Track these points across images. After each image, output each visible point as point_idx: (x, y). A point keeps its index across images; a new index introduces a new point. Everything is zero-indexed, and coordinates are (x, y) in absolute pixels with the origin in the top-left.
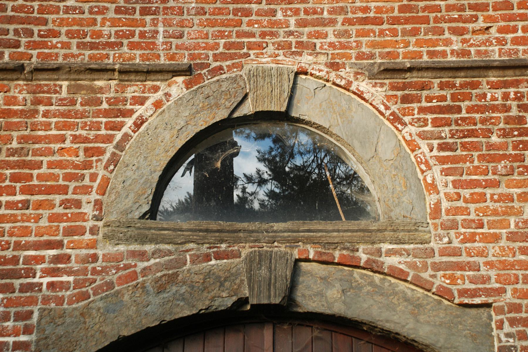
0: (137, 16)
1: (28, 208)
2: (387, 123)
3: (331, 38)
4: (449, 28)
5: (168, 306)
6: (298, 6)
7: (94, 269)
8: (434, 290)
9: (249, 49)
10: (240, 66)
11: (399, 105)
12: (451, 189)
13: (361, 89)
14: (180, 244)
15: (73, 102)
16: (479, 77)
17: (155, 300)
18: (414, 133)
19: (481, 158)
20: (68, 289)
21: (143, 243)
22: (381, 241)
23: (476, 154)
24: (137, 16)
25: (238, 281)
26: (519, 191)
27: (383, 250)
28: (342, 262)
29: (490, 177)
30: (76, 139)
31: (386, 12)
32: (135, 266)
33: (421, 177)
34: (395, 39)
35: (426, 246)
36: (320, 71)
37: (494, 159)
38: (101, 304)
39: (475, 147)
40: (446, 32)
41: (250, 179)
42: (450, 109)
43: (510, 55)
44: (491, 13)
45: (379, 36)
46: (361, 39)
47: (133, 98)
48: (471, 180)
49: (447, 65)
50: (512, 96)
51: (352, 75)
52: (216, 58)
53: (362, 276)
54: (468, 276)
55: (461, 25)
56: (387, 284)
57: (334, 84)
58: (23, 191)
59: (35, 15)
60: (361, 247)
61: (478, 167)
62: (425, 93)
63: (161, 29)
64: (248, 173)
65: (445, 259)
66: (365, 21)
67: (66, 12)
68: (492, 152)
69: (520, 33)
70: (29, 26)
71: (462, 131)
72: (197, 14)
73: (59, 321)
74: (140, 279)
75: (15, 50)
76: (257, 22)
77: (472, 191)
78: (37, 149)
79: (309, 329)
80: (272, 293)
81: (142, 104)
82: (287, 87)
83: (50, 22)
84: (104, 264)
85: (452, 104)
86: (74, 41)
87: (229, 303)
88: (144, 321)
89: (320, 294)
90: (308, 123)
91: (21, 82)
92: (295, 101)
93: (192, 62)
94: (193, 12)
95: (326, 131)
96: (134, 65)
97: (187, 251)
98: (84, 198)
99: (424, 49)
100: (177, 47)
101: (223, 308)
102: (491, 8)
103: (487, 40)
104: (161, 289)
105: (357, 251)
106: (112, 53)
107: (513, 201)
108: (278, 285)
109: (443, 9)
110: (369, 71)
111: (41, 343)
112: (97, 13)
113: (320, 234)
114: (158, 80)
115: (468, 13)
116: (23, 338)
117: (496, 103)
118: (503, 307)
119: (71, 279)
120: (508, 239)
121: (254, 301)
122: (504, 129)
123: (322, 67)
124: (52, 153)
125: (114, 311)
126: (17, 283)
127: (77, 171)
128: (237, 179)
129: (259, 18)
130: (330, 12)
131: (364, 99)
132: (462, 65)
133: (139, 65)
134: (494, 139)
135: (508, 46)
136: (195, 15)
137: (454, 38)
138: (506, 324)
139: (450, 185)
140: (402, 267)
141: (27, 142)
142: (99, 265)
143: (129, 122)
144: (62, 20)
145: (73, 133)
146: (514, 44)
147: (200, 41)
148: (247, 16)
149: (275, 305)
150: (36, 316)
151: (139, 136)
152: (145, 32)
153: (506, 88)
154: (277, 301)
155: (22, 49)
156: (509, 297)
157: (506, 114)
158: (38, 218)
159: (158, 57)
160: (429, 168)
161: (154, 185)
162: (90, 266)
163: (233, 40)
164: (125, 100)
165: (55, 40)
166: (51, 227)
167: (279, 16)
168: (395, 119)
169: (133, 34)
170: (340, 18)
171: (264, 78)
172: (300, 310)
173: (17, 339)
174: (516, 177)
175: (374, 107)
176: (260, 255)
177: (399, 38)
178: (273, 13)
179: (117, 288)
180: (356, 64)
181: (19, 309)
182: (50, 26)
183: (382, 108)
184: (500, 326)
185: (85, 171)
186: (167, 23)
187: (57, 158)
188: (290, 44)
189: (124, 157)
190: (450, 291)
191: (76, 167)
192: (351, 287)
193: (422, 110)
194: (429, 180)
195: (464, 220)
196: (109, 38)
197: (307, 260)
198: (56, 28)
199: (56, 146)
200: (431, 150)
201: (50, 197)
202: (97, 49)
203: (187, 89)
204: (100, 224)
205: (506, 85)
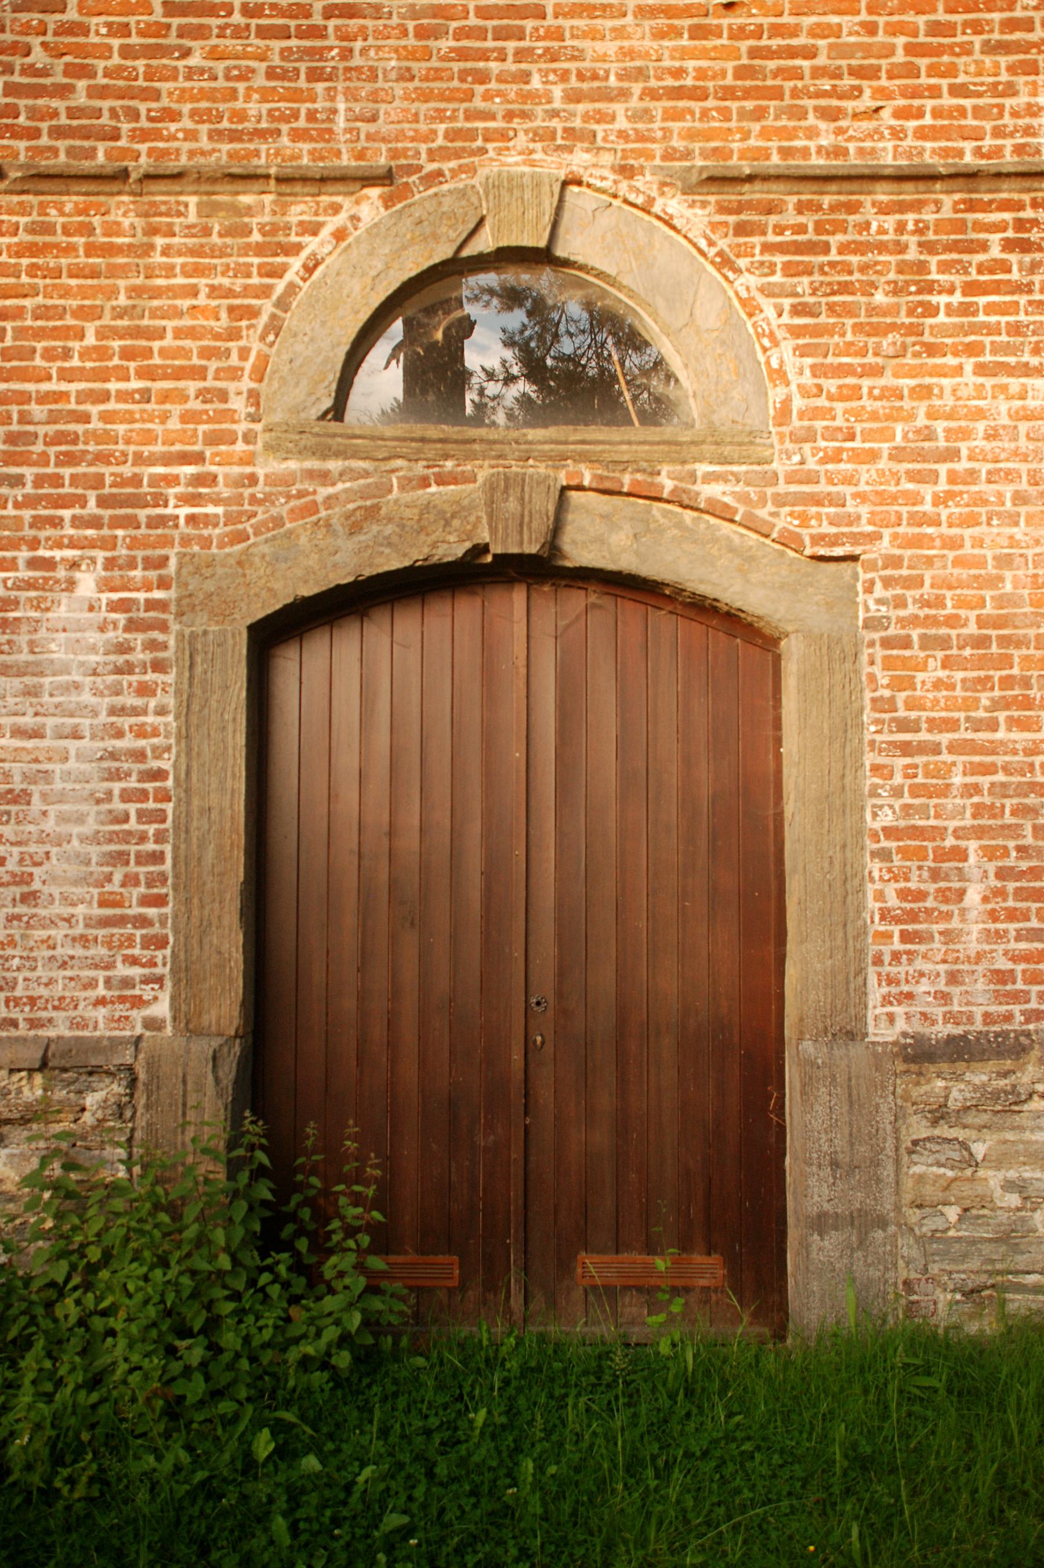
0: (302, 83)
1: (148, 401)
2: (710, 268)
3: (622, 123)
4: (816, 109)
5: (367, 554)
6: (566, 65)
7: (253, 496)
8: (774, 535)
9: (486, 140)
10: (472, 170)
11: (731, 239)
12: (807, 379)
13: (669, 210)
14: (384, 459)
15: (207, 232)
16: (861, 193)
18: (753, 286)
19: (858, 328)
20: (216, 525)
21: (324, 457)
22: (695, 460)
23: (849, 322)
24: (302, 83)
25: (472, 519)
26: (912, 382)
27: (699, 474)
28: (635, 491)
29: (870, 359)
30: (214, 291)
31: (714, 78)
32: (315, 492)
33: (762, 359)
34: (726, 125)
35: (766, 467)
36: (603, 179)
38: (266, 549)
39: (849, 310)
40: (811, 115)
41: (490, 376)
42: (811, 248)
43: (910, 156)
44: (884, 82)
45: (701, 119)
46: (670, 124)
47: (301, 223)
48: (841, 365)
49: (810, 172)
50: (910, 226)
51: (655, 187)
52: (432, 154)
53: (665, 513)
54: (828, 515)
55: (835, 102)
56: (703, 526)
57: (626, 201)
58: (141, 374)
59: (141, 82)
60: (665, 469)
61: (851, 344)
62: (773, 219)
63: (341, 106)
64: (488, 366)
65: (793, 488)
66: (677, 93)
67: (188, 78)
68: (874, 320)
69: (928, 120)
70: (131, 103)
71: (830, 284)
72: (401, 78)
73: (207, 572)
74: (323, 513)
75: (112, 144)
76: (499, 93)
77: (841, 382)
78: (157, 308)
79: (582, 593)
80: (526, 537)
81: (315, 234)
82: (548, 206)
83: (164, 94)
84: (268, 489)
85: (815, 238)
86: (204, 128)
87: (459, 551)
88: (331, 576)
89: (601, 540)
90: (582, 268)
91: (126, 198)
92: (562, 230)
93: (393, 163)
94: (393, 75)
95: (612, 281)
96: (300, 167)
97: (393, 471)
98: (231, 386)
99: (774, 144)
100: (369, 137)
101: (450, 559)
102: (883, 74)
103: (876, 131)
104: (355, 529)
105: (659, 473)
106: (263, 147)
107: (901, 398)
108: (534, 525)
109: (807, 73)
110: (684, 180)
111: (185, 602)
112: (240, 78)
113: (600, 448)
114: (339, 194)
115: (848, 82)
116: (158, 594)
117: (885, 238)
118: (875, 560)
119: (220, 510)
120: (891, 457)
121: (497, 549)
122: (895, 282)
123: (606, 173)
124: (179, 314)
125: (286, 560)
126: (142, 514)
127: (218, 344)
128: (471, 374)
129: (503, 86)
130: (620, 77)
131: (673, 228)
132: (833, 172)
133: (308, 167)
134: (880, 298)
135: (910, 142)
136: (397, 80)
137: (823, 125)
138: (879, 585)
139: (807, 372)
140: (727, 499)
141: (140, 297)
142: (260, 490)
143: (296, 264)
144: (183, 90)
145: (210, 282)
146: (918, 138)
147: (406, 126)
148: (482, 83)
149: (530, 556)
150: (173, 563)
151: (313, 287)
152: (316, 111)
153: (901, 212)
154: (532, 549)
155: (123, 143)
156: (885, 545)
157: (900, 257)
158: (164, 417)
159: (338, 154)
160: (776, 343)
161: (339, 367)
162: (247, 492)
163: (459, 125)
164: (288, 227)
165: (173, 127)
166: (185, 431)
167: (536, 83)
168: (724, 262)
169: (295, 115)
170: (637, 88)
171: (510, 190)
172: (568, 564)
173: (149, 595)
174: (909, 360)
175: (690, 241)
176: (507, 479)
177: (733, 124)
178: (525, 77)
179: (288, 526)
180: (661, 168)
181: (149, 552)
182: (165, 102)
183: (703, 244)
184: (869, 589)
185: (231, 344)
186: (352, 96)
187: (187, 322)
188: (554, 132)
189: (290, 320)
190: (798, 538)
191: (217, 337)
192: (648, 530)
193: (767, 248)
194: (775, 364)
195: (826, 428)
196: (259, 121)
197: (580, 488)
198: (174, 106)
199: (185, 303)
200: (780, 315)
201: (181, 384)
202: (240, 140)
203: (387, 208)
204: (258, 427)
205: (902, 207)
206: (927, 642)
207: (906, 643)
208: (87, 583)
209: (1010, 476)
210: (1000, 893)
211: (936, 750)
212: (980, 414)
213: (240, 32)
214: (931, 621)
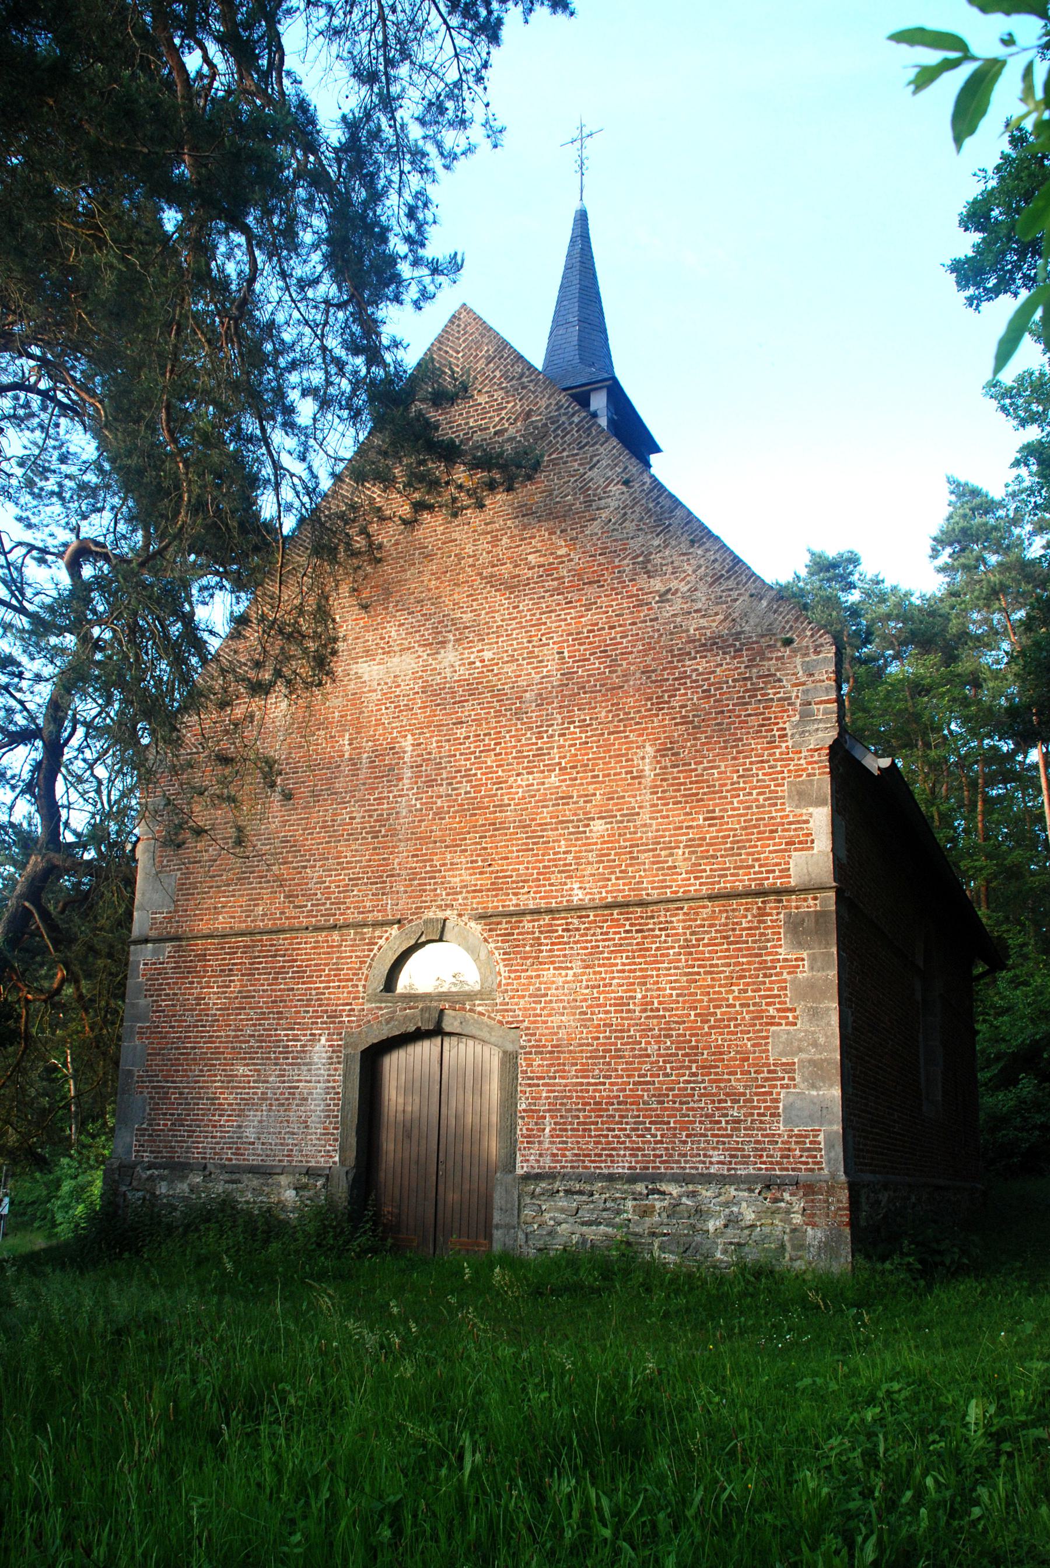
17: (386, 1028)
37: (526, 958)
39: (518, 953)
66: (475, 891)
104: (388, 1023)
134: (528, 948)
156: (526, 1024)
189: (374, 964)
205: (534, 921)
206: (536, 1053)
207: (530, 1053)
208: (323, 1039)
209: (562, 1001)
210: (554, 1129)
211: (538, 1085)
212: (553, 982)
213: (366, 884)
214: (538, 1046)
